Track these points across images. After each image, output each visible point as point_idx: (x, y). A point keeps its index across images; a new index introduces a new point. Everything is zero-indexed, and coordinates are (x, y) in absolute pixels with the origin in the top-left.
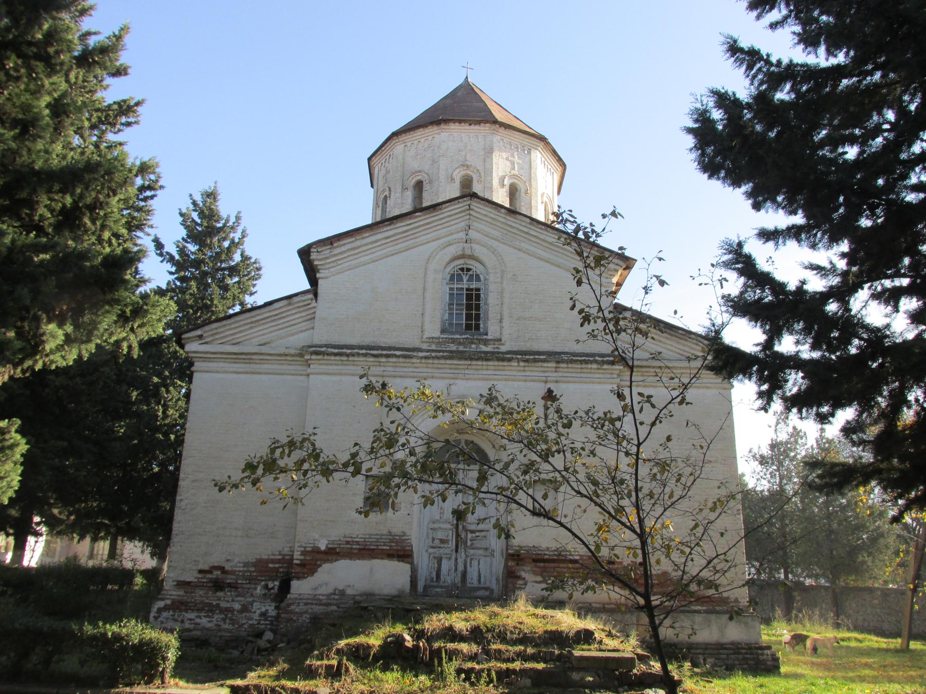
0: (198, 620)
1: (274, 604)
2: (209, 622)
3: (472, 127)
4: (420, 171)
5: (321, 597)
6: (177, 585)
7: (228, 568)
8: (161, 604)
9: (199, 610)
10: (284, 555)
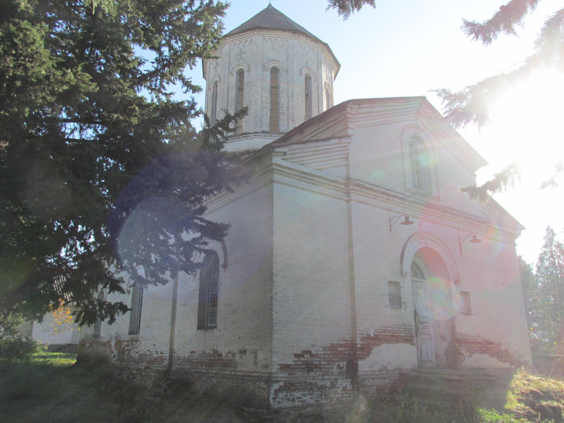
0: (304, 398)
1: (349, 380)
2: (311, 398)
3: (313, 43)
4: (278, 61)
5: (378, 373)
6: (281, 368)
7: (314, 352)
8: (276, 386)
9: (304, 389)
10: (346, 341)
